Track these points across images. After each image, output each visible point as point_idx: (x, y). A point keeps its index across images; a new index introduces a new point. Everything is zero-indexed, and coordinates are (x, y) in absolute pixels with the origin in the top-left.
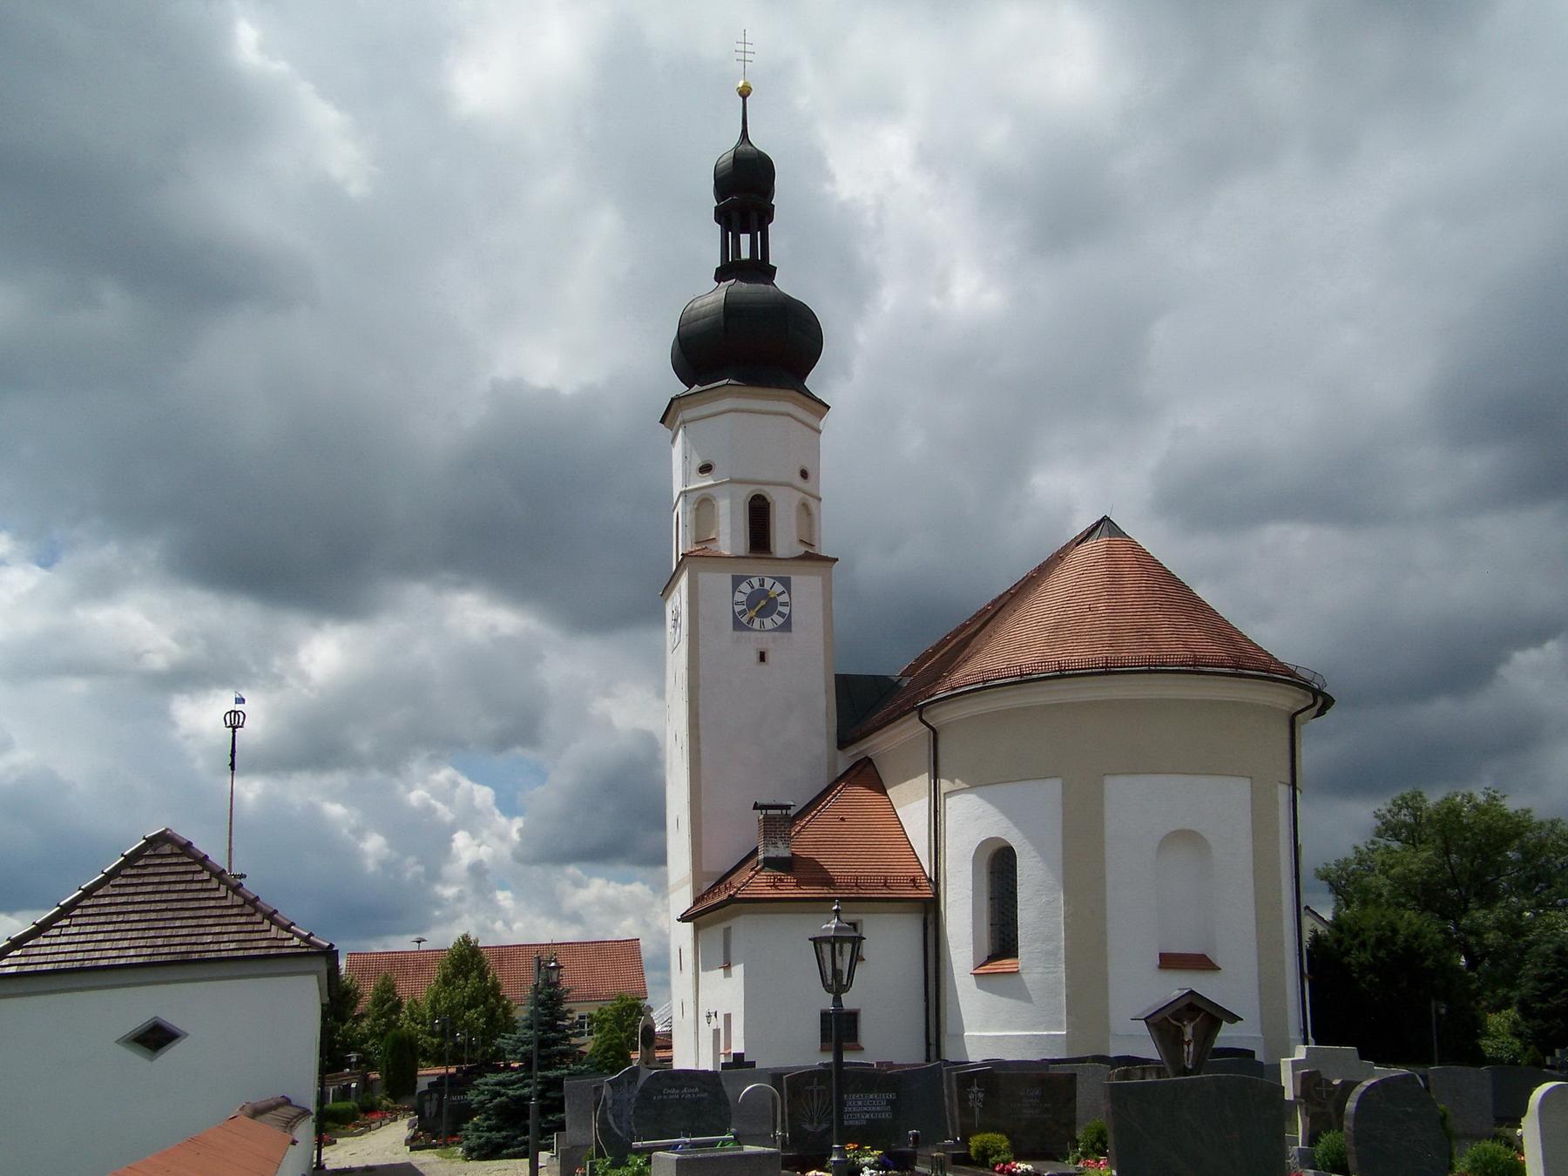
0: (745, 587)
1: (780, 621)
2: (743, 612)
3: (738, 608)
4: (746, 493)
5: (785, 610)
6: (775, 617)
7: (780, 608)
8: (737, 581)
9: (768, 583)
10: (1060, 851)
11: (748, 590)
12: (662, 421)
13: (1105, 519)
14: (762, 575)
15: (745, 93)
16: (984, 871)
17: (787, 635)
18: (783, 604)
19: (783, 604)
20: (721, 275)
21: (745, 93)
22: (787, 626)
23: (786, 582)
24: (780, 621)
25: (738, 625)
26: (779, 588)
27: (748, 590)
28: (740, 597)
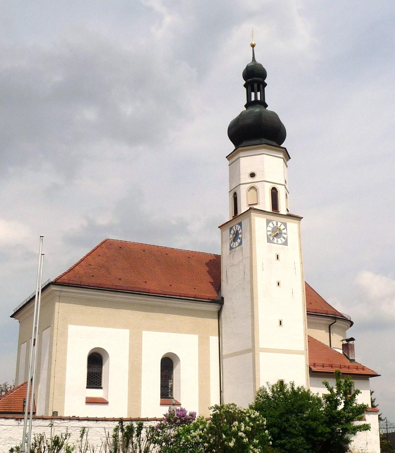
0: (271, 224)
1: (284, 240)
2: (270, 235)
3: (269, 233)
4: (270, 186)
5: (285, 236)
6: (282, 238)
7: (283, 235)
8: (268, 222)
9: (279, 224)
10: (139, 312)
11: (272, 226)
12: (226, 157)
13: (290, 158)
14: (277, 221)
15: (253, 46)
16: (313, 377)
17: (286, 246)
18: (285, 234)
19: (285, 234)
20: (246, 106)
21: (253, 46)
22: (286, 243)
23: (285, 224)
24: (284, 240)
25: (269, 241)
26: (282, 227)
27: (272, 226)
28: (269, 229)
